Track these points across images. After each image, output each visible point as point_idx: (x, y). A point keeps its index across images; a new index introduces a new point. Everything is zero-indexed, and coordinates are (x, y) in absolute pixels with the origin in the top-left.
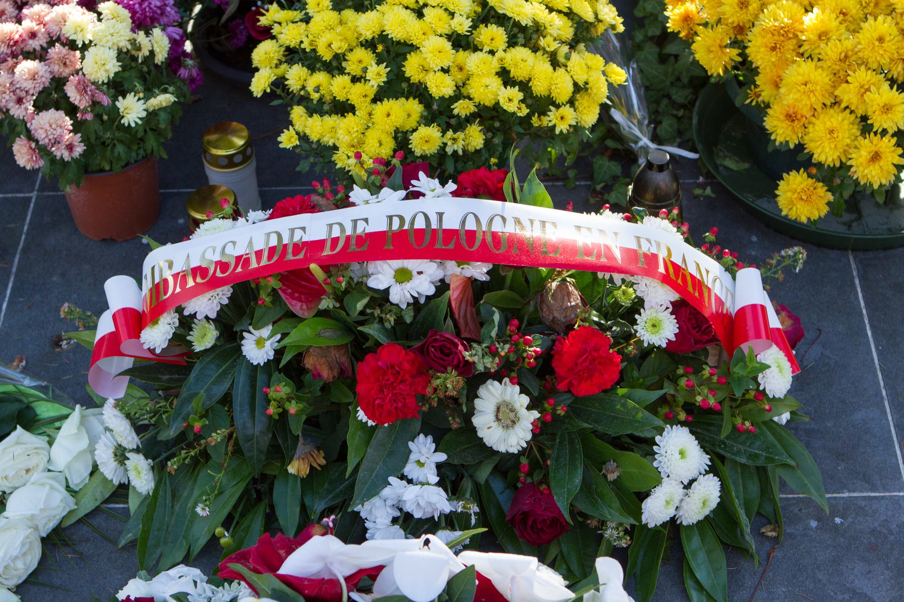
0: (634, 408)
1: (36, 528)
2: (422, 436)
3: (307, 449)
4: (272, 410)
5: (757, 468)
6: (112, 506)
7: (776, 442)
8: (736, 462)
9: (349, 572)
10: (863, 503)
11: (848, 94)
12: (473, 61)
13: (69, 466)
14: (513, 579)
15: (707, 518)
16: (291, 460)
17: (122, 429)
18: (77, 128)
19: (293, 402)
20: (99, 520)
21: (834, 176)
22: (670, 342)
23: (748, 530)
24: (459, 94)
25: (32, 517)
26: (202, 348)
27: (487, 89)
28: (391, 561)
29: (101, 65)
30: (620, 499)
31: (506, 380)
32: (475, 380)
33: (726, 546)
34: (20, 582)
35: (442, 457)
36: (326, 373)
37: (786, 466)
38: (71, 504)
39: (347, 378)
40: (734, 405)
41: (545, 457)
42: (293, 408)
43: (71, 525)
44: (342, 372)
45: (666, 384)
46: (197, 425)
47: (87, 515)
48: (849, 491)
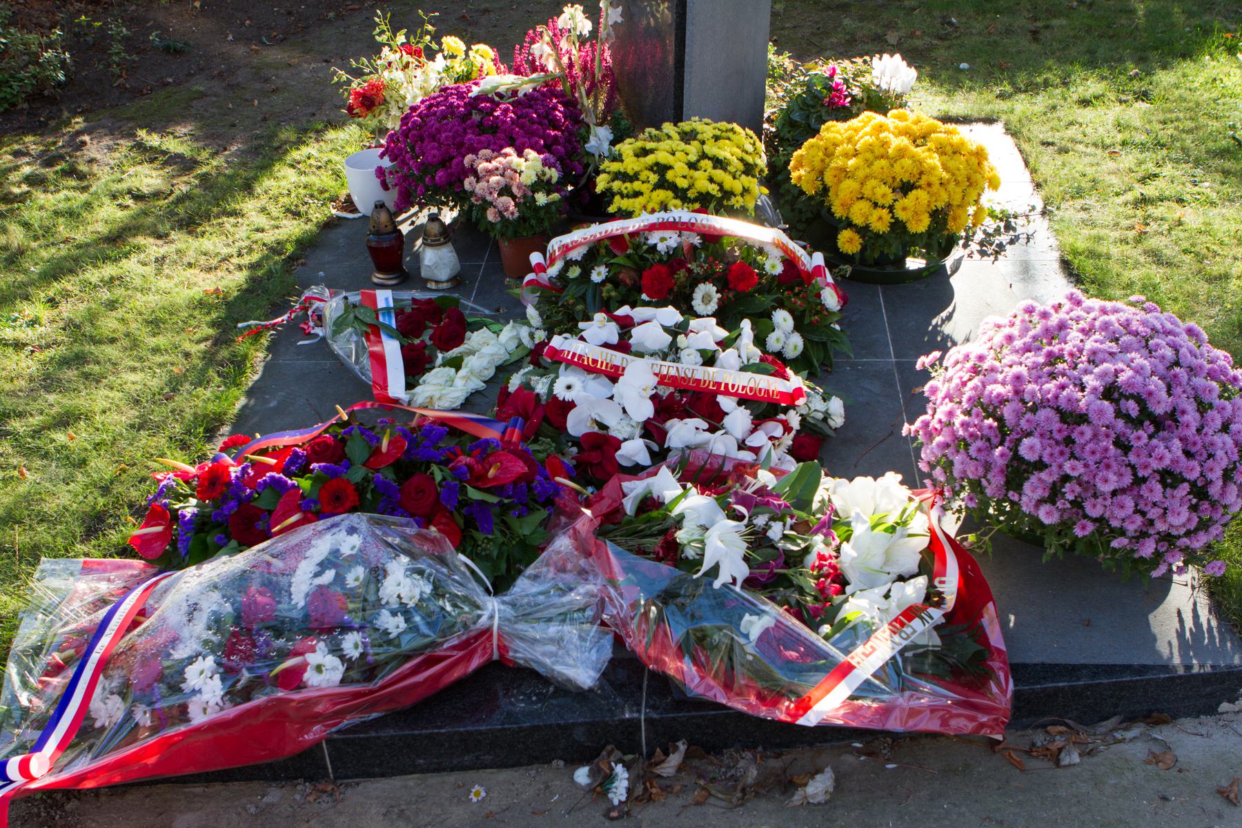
11: (867, 191)
12: (697, 174)
18: (516, 205)
21: (864, 231)
24: (691, 186)
27: (703, 185)
29: (528, 177)
32: (695, 281)
36: (628, 281)
38: (508, 357)
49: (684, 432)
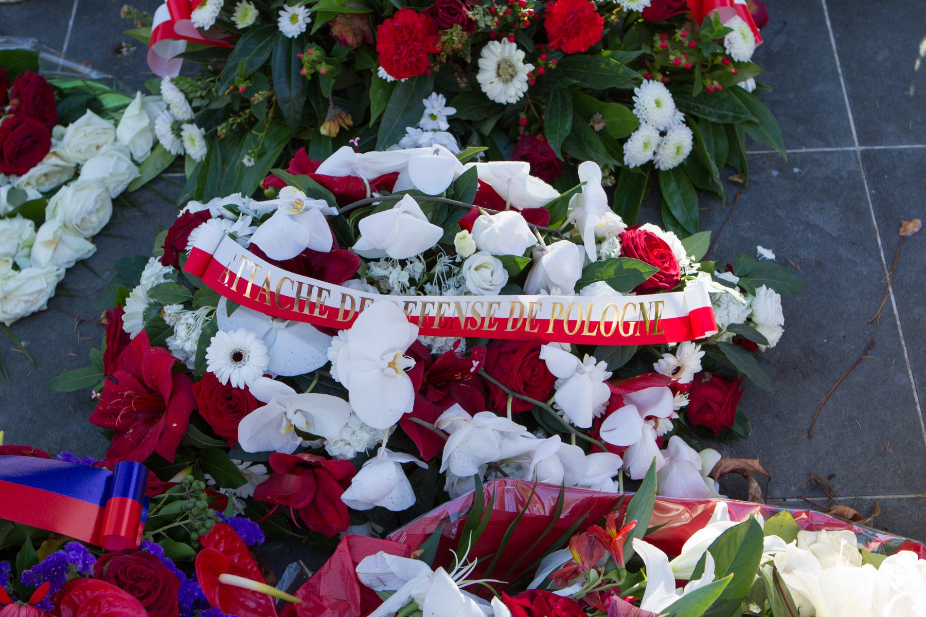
0: (616, 65)
1: (107, 190)
2: (434, 94)
3: (337, 111)
4: (305, 71)
5: (725, 125)
6: (171, 175)
7: (742, 105)
8: (706, 121)
9: (374, 176)
10: (819, 156)
13: (132, 142)
14: (509, 180)
15: (681, 165)
16: (323, 122)
17: (178, 100)
19: (324, 64)
20: (159, 187)
22: (646, 9)
23: (718, 177)
25: (103, 180)
26: (245, 25)
28: (405, 167)
30: (606, 147)
31: (505, 39)
32: (480, 39)
33: (698, 190)
34: (96, 233)
35: (452, 111)
36: (350, 39)
37: (750, 123)
38: (135, 172)
39: (368, 46)
40: (705, 70)
41: (540, 113)
42: (323, 68)
43: (136, 191)
44: (365, 39)
45: (644, 46)
46: (242, 86)
47: (150, 182)
48: (806, 147)
49: (476, 439)
